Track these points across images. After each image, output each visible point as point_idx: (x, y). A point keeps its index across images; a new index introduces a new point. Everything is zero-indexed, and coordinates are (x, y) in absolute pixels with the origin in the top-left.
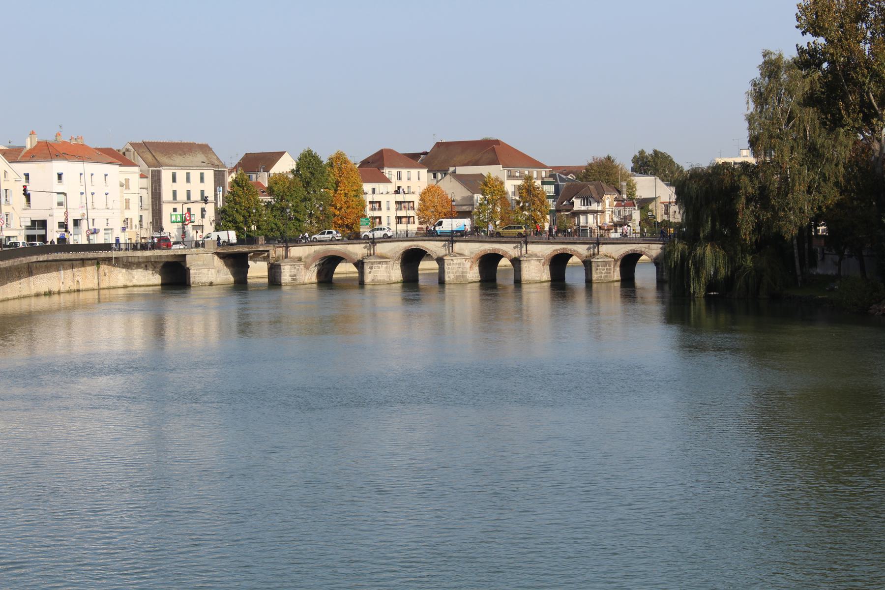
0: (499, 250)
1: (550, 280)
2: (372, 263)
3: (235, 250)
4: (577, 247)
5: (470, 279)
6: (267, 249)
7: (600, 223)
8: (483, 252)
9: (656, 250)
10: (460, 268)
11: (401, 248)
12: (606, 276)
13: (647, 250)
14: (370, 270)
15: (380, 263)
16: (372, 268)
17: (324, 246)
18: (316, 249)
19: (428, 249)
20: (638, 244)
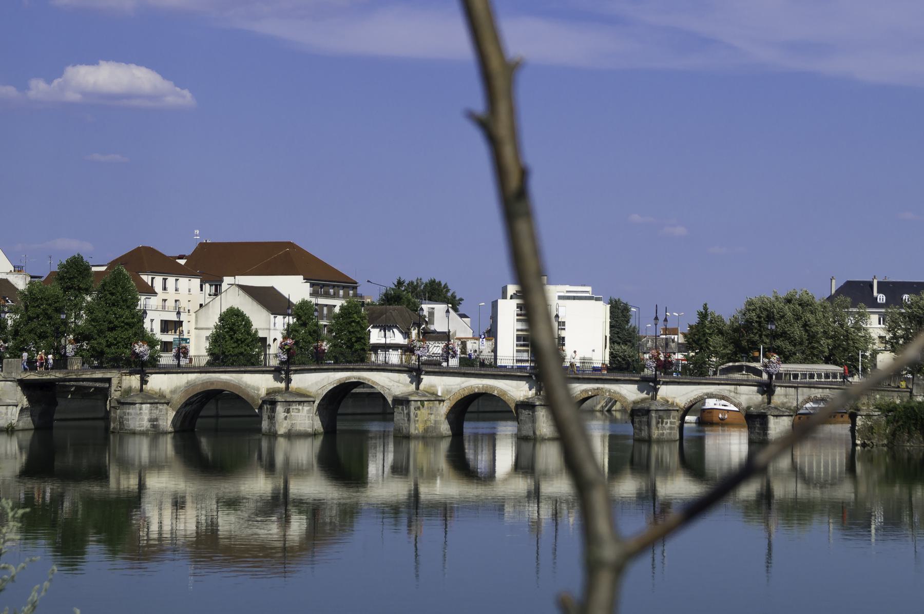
0: (492, 388)
1: (451, 434)
2: (289, 403)
3: (48, 377)
4: (620, 386)
5: (444, 432)
6: (108, 375)
7: (405, 362)
8: (467, 391)
9: (747, 394)
10: (431, 414)
11: (331, 380)
12: (670, 434)
13: (732, 394)
14: (286, 414)
15: (300, 403)
16: (288, 411)
17: (203, 375)
18: (190, 379)
19: (377, 384)
20: (719, 384)
